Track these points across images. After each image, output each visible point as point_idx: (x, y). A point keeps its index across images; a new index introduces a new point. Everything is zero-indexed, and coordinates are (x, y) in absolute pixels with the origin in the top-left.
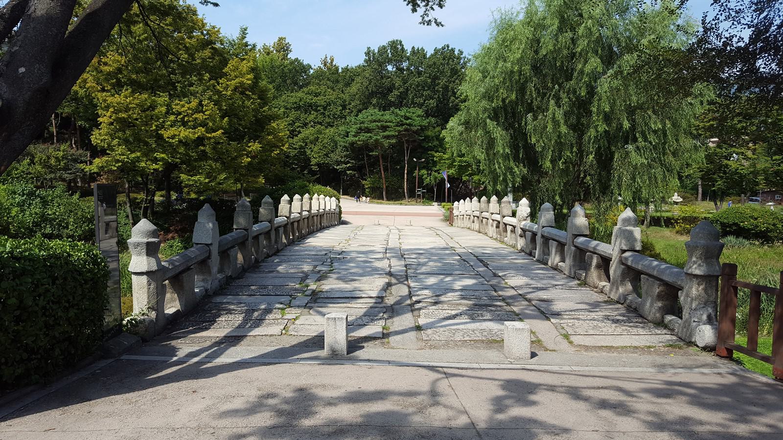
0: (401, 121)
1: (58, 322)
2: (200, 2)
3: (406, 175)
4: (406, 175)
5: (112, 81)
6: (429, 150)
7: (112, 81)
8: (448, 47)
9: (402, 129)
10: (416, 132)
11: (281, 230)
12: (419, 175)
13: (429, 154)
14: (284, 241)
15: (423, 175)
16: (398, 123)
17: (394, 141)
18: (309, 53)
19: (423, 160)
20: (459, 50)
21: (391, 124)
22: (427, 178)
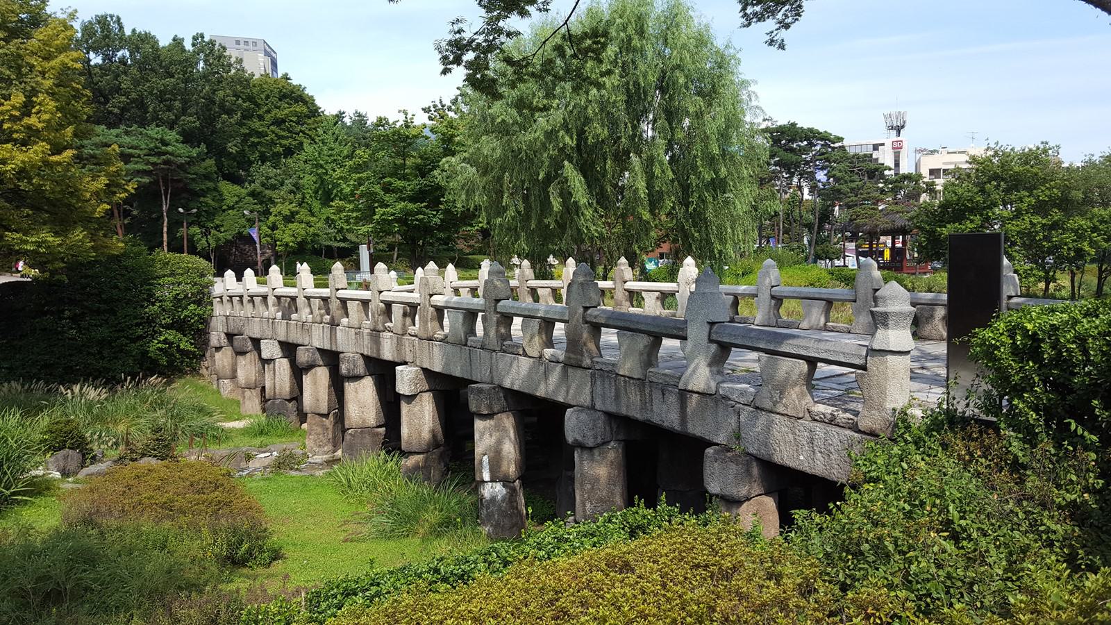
0: (157, 147)
1: (597, 258)
2: (423, 109)
3: (165, 235)
4: (165, 235)
5: (806, 191)
6: (200, 196)
7: (806, 191)
8: (202, 37)
9: (159, 161)
10: (181, 166)
11: (236, 300)
12: (188, 235)
13: (201, 203)
14: (892, 172)
15: (194, 235)
16: (150, 150)
17: (146, 180)
18: (328, 105)
19: (195, 211)
20: (220, 45)
21: (138, 151)
22: (201, 240)
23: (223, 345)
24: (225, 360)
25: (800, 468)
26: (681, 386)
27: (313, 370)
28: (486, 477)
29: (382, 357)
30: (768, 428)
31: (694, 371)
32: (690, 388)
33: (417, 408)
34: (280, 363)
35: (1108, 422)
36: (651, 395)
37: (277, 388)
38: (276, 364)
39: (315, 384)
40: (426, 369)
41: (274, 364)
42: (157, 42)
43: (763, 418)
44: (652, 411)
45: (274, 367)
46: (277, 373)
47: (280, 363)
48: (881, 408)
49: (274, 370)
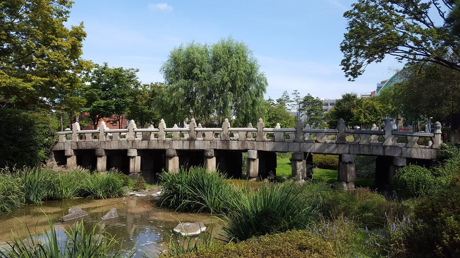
23: (72, 154)
24: (72, 162)
25: (235, 149)
26: (383, 145)
27: (174, 158)
28: (301, 177)
29: (413, 157)
30: (411, 151)
31: (388, 141)
32: (386, 145)
33: (255, 163)
34: (138, 158)
35: (35, 1)
36: (372, 148)
37: (136, 168)
38: (136, 158)
39: (174, 162)
40: (216, 149)
41: (135, 158)
42: (261, 89)
43: (409, 149)
44: (373, 152)
45: (135, 159)
46: (136, 162)
47: (138, 158)
48: (438, 144)
49: (135, 161)
